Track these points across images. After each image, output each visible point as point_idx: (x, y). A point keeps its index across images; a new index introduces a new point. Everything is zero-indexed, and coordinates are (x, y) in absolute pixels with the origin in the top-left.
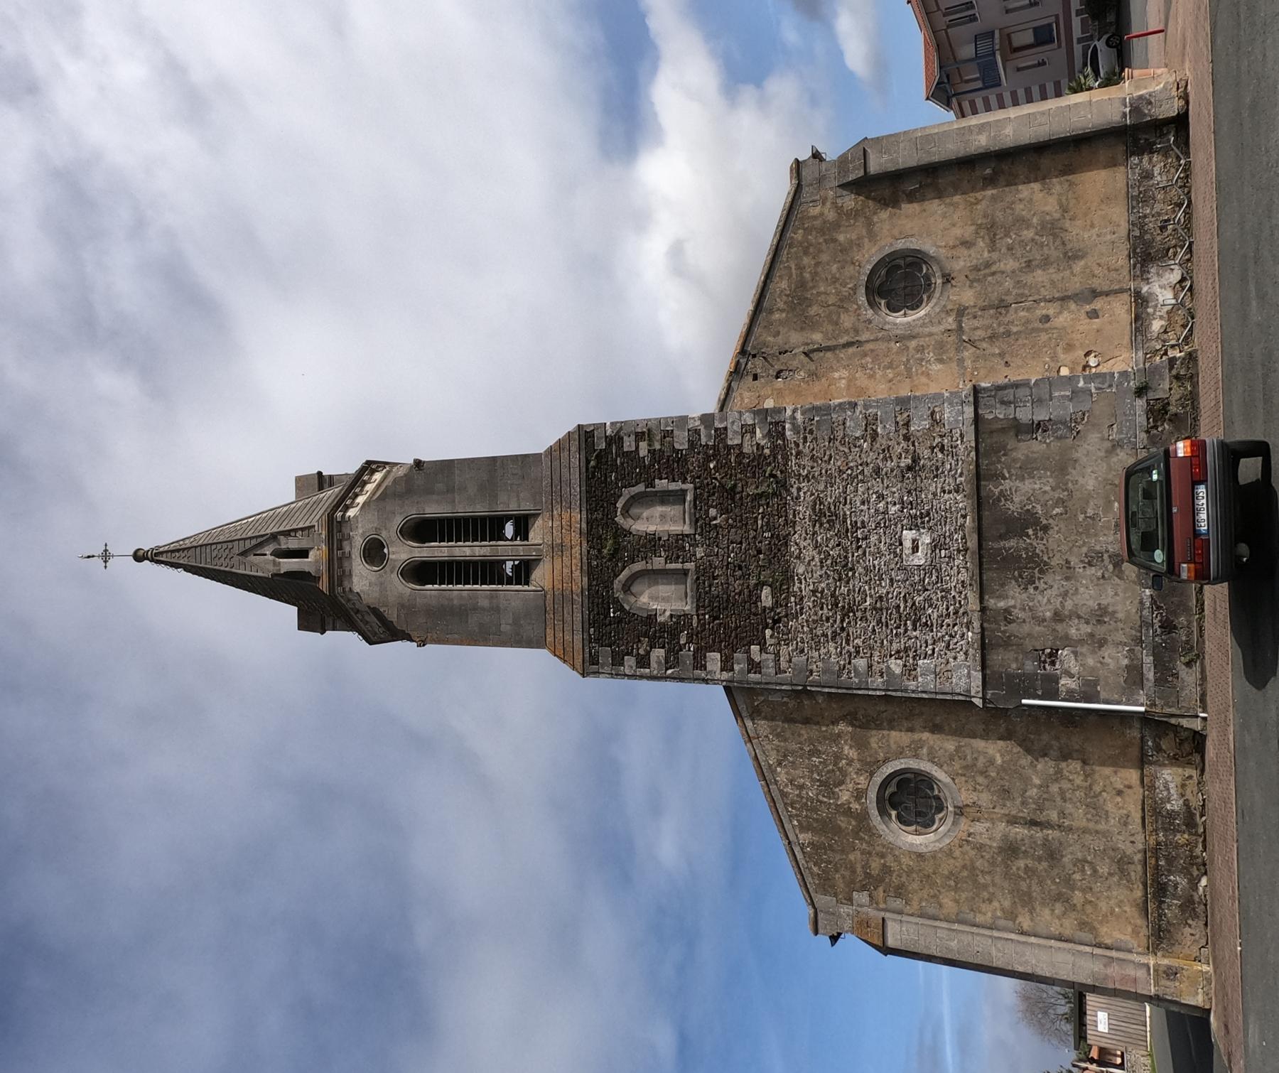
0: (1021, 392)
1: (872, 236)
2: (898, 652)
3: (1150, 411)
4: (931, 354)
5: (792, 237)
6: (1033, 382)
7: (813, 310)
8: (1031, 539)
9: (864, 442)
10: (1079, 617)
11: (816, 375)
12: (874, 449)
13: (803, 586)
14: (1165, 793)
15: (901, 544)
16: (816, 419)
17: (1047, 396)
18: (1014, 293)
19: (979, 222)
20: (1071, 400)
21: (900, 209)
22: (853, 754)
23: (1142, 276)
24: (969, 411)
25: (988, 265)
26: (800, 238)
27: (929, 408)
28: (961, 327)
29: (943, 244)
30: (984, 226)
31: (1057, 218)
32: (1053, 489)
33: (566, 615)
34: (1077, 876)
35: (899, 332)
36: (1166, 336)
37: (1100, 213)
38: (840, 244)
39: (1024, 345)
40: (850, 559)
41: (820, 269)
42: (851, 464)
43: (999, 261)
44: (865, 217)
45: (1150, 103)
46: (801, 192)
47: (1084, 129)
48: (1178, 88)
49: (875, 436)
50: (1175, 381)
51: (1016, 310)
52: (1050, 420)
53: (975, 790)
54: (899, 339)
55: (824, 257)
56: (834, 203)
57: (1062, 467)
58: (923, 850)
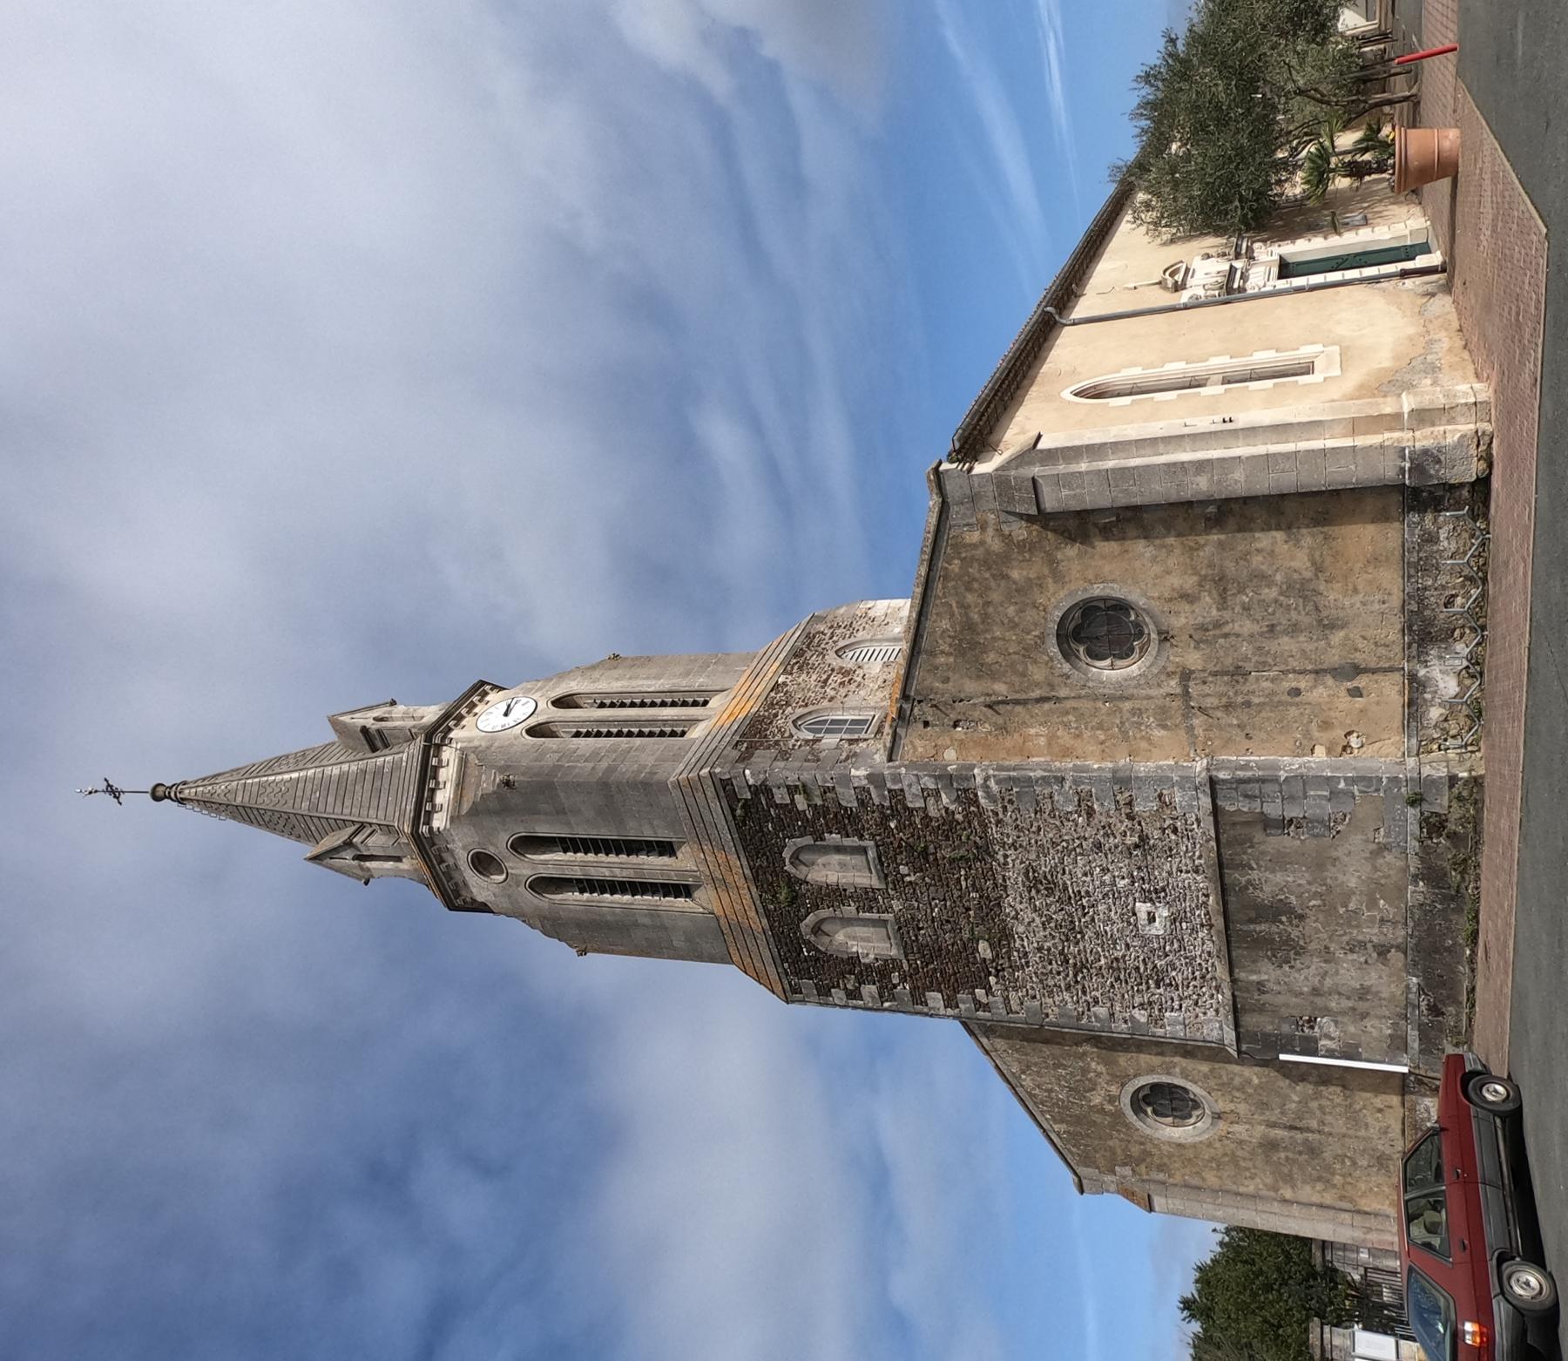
0: (1268, 788)
1: (1058, 576)
2: (1142, 1004)
3: (1424, 821)
4: (1152, 720)
5: (946, 568)
6: (1282, 779)
7: (991, 657)
8: (1285, 926)
9: (1079, 816)
10: (1339, 994)
11: (1006, 729)
12: (1092, 824)
13: (1026, 944)
14: (1426, 1115)
15: (1134, 914)
16: (1015, 790)
17: (1301, 794)
18: (1253, 660)
19: (1203, 572)
20: (1329, 800)
21: (1094, 547)
22: (1100, 1068)
23: (1419, 657)
24: (1206, 801)
25: (1218, 625)
26: (957, 570)
27: (1156, 790)
28: (1188, 692)
29: (1156, 595)
30: (1209, 578)
31: (1308, 577)
32: (1309, 883)
33: (750, 946)
34: (1338, 1166)
35: (1106, 691)
36: (1446, 725)
37: (1365, 576)
38: (1015, 583)
39: (1268, 719)
40: (1077, 923)
41: (991, 610)
42: (1066, 838)
43: (1233, 621)
44: (1045, 552)
45: (1439, 462)
46: (948, 512)
47: (1345, 484)
48: (1478, 446)
49: (1090, 813)
50: (1455, 801)
51: (1257, 679)
52: (1304, 817)
53: (1232, 1101)
54: (1107, 699)
55: (995, 596)
56: (999, 531)
57: (1320, 864)
58: (1183, 1141)
